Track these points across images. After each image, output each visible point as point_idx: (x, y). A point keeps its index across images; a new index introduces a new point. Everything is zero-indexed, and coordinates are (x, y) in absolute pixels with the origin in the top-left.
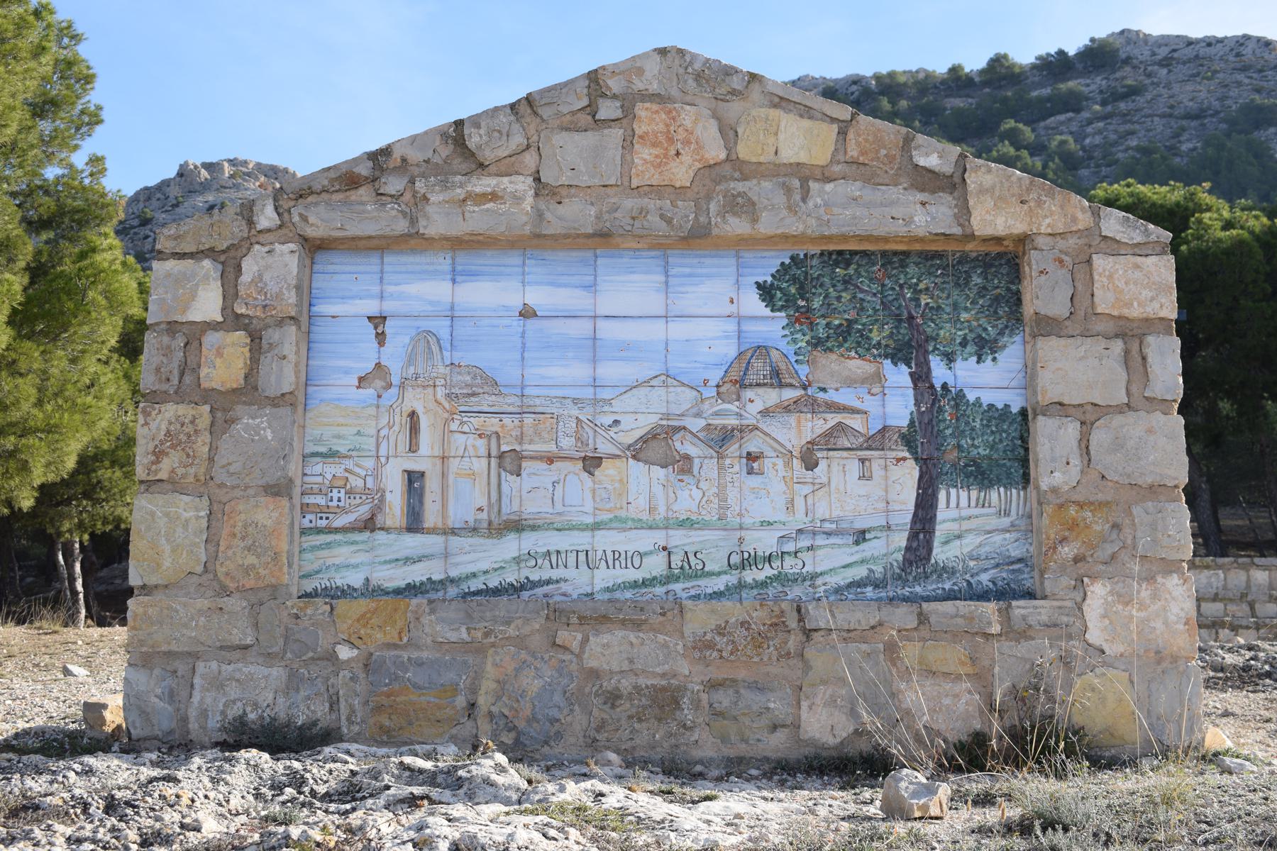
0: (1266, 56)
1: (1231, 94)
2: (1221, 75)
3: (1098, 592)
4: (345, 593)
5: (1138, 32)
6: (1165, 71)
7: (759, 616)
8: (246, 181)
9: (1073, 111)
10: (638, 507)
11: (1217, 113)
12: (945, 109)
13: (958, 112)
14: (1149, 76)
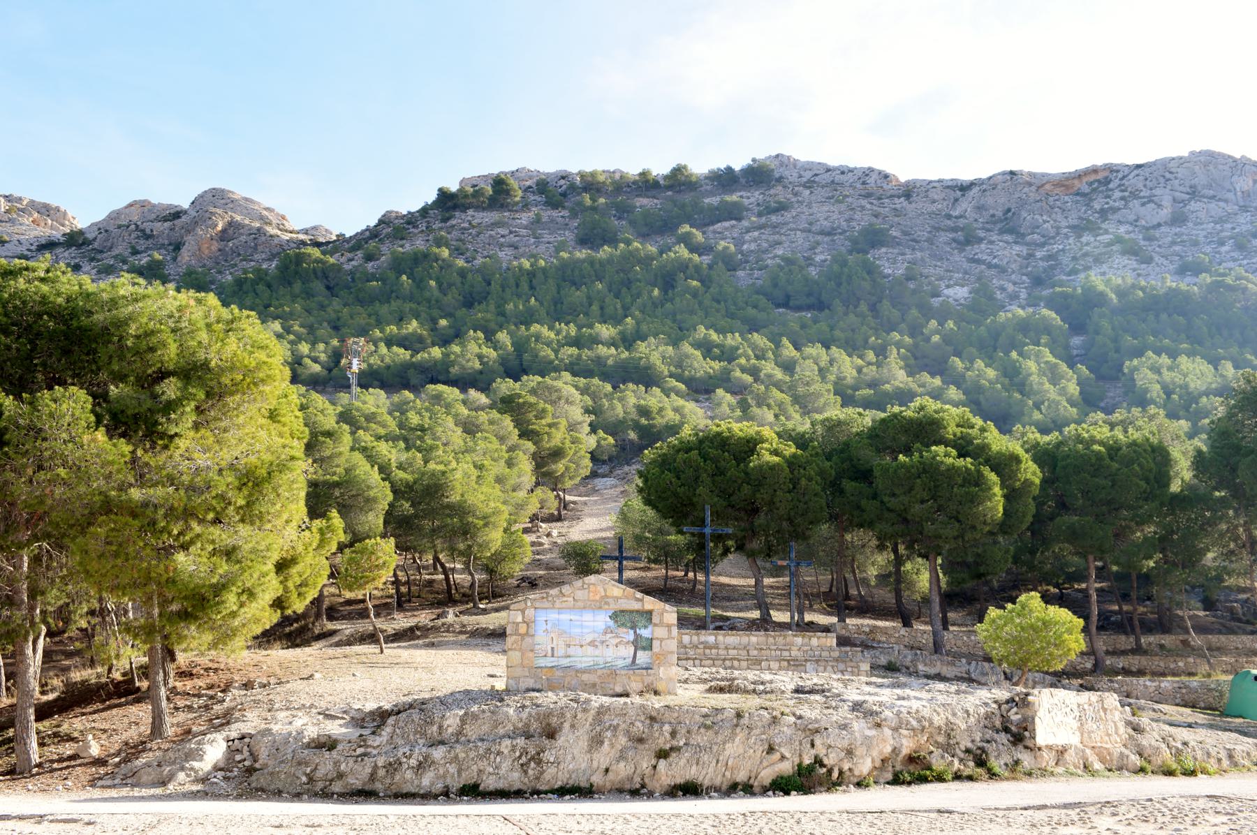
0: (885, 186)
1: (856, 216)
2: (850, 200)
3: (662, 669)
4: (541, 667)
5: (789, 158)
6: (808, 192)
7: (609, 672)
8: (21, 216)
9: (736, 219)
10: (589, 654)
11: (845, 231)
12: (636, 207)
13: (647, 214)
14: (796, 194)
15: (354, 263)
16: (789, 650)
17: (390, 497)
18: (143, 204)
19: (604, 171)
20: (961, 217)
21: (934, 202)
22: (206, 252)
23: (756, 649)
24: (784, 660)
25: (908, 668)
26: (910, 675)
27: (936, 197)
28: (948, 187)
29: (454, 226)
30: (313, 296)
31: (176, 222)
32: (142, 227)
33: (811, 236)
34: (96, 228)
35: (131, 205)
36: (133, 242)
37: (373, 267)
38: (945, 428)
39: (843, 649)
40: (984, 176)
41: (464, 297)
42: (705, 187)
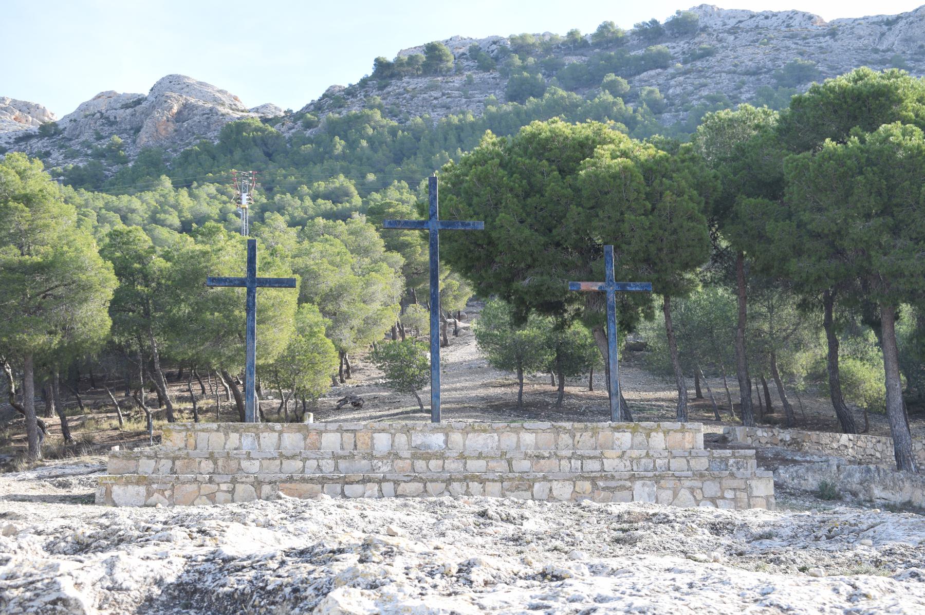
0: (810, 28)
1: (781, 56)
2: (775, 42)
5: (712, 7)
6: (732, 37)
8: (4, 115)
9: (661, 68)
11: (770, 70)
14: (720, 41)
15: (293, 131)
16: (600, 458)
17: (114, 283)
18: (109, 95)
19: (534, 35)
20: (888, 50)
21: (860, 38)
22: (163, 133)
23: (527, 456)
24: (585, 478)
25: (855, 494)
26: (860, 505)
27: (862, 33)
28: (874, 23)
29: (389, 93)
30: (252, 162)
31: (136, 108)
32: (106, 115)
33: (736, 77)
34: (68, 120)
35: (98, 97)
36: (99, 129)
37: (311, 133)
38: (900, 101)
39: (717, 453)
40: (910, 9)
41: (395, 155)
42: (631, 42)
